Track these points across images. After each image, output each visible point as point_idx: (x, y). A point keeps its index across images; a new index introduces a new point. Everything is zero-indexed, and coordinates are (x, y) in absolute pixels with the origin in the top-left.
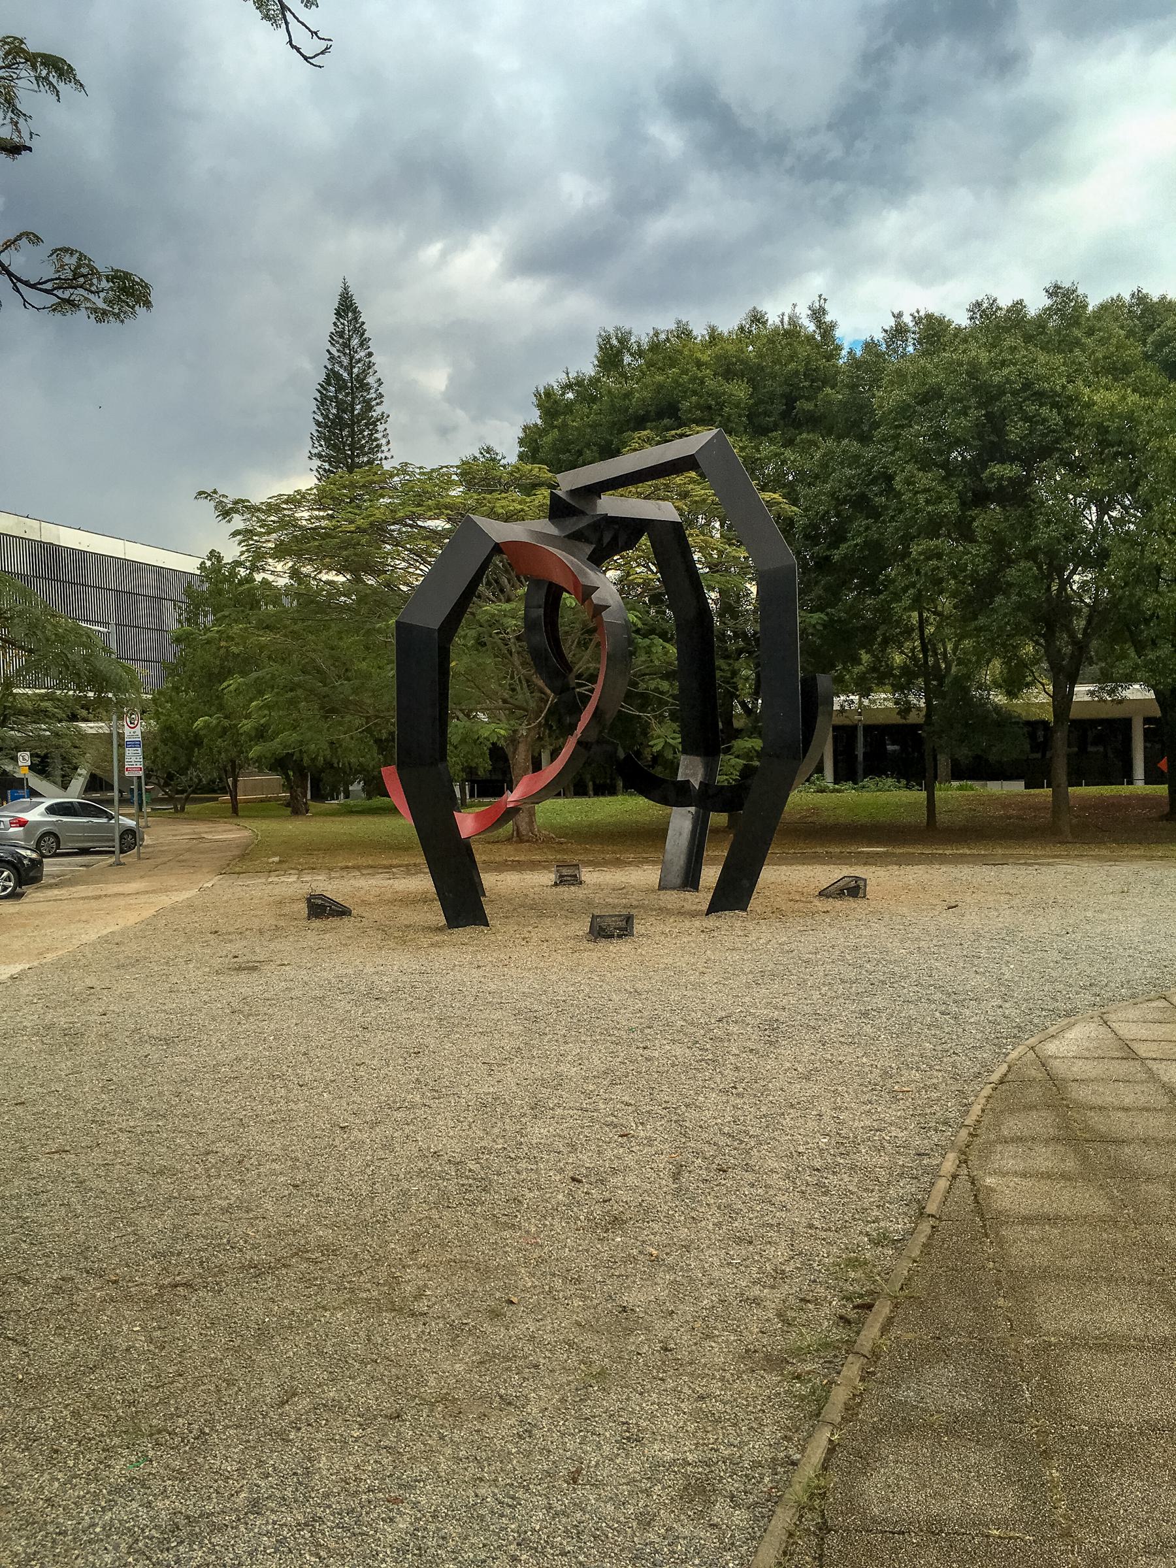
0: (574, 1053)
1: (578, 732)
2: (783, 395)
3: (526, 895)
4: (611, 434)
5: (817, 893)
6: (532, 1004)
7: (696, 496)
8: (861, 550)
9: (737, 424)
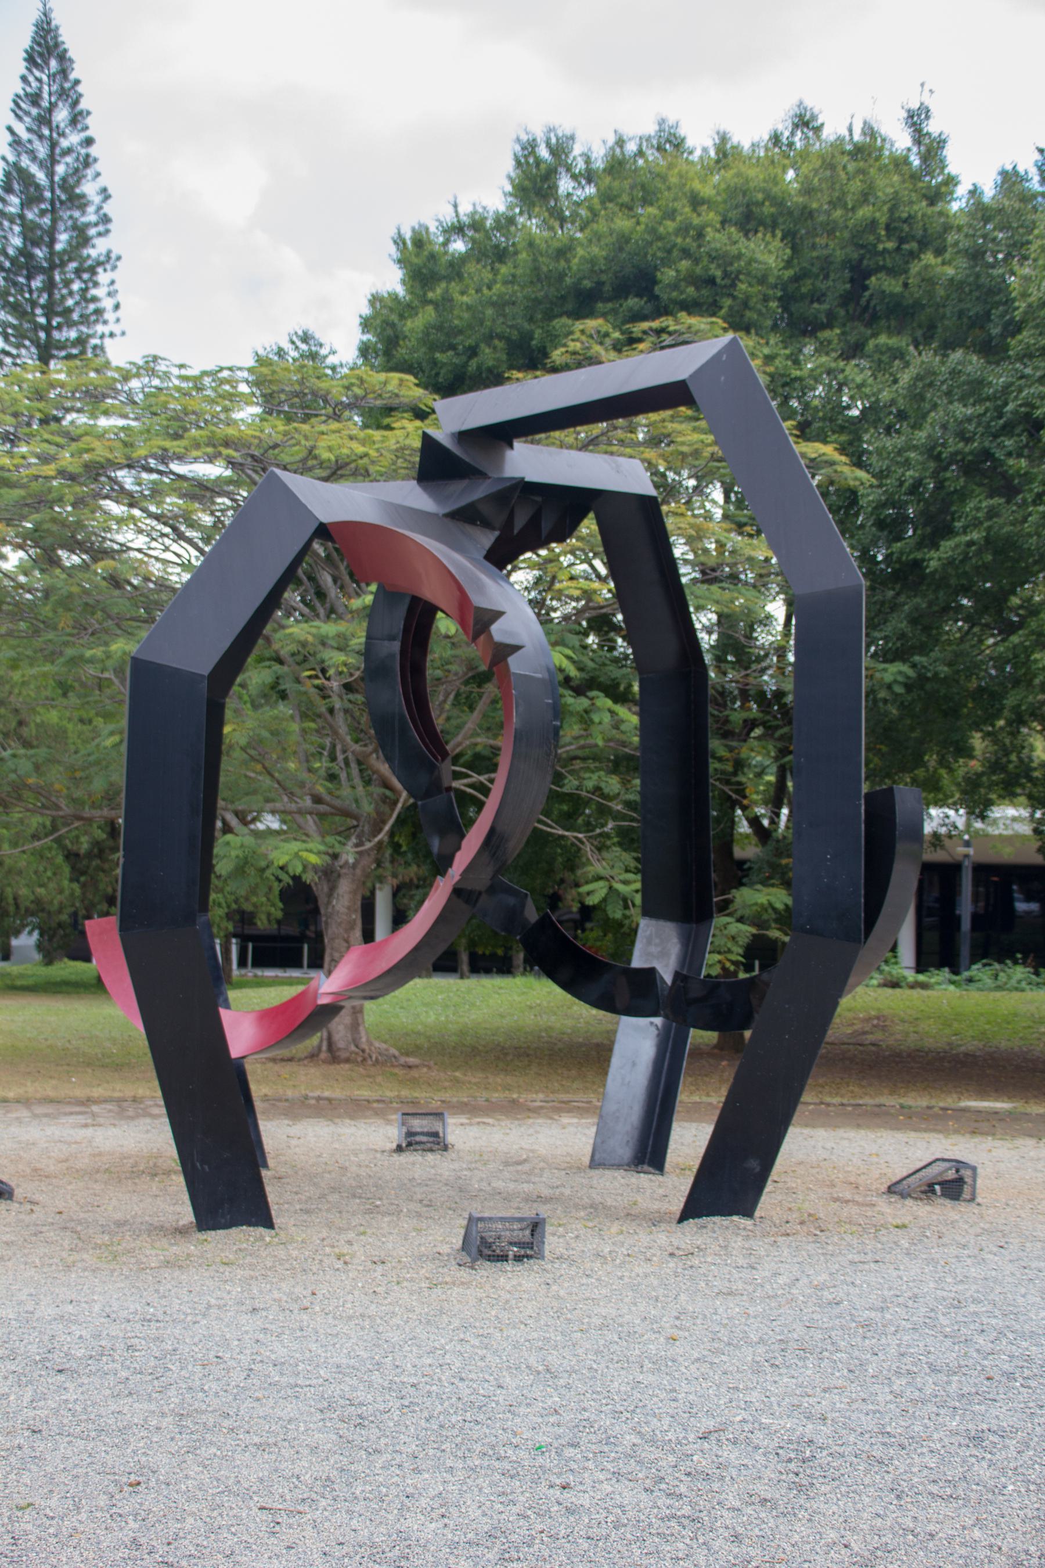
0: (432, 1493)
1: (456, 871)
2: (847, 263)
3: (344, 1169)
4: (531, 320)
5: (884, 1188)
6: (354, 1389)
7: (683, 443)
8: (979, 553)
9: (760, 313)
